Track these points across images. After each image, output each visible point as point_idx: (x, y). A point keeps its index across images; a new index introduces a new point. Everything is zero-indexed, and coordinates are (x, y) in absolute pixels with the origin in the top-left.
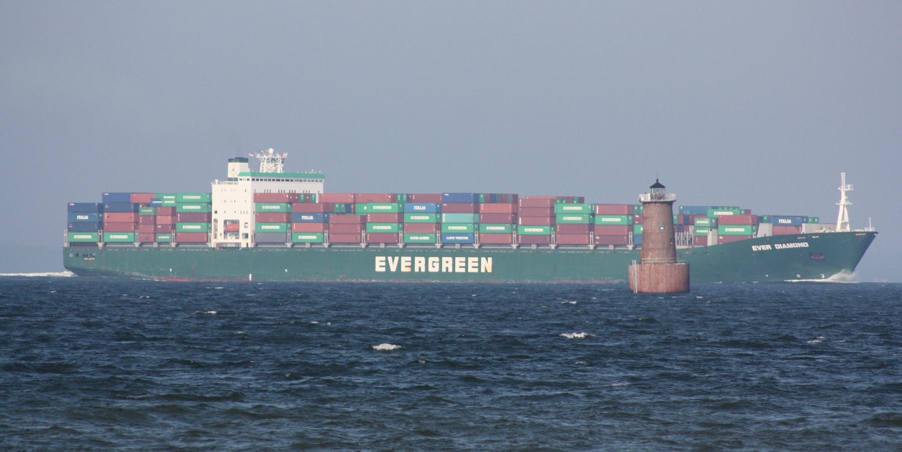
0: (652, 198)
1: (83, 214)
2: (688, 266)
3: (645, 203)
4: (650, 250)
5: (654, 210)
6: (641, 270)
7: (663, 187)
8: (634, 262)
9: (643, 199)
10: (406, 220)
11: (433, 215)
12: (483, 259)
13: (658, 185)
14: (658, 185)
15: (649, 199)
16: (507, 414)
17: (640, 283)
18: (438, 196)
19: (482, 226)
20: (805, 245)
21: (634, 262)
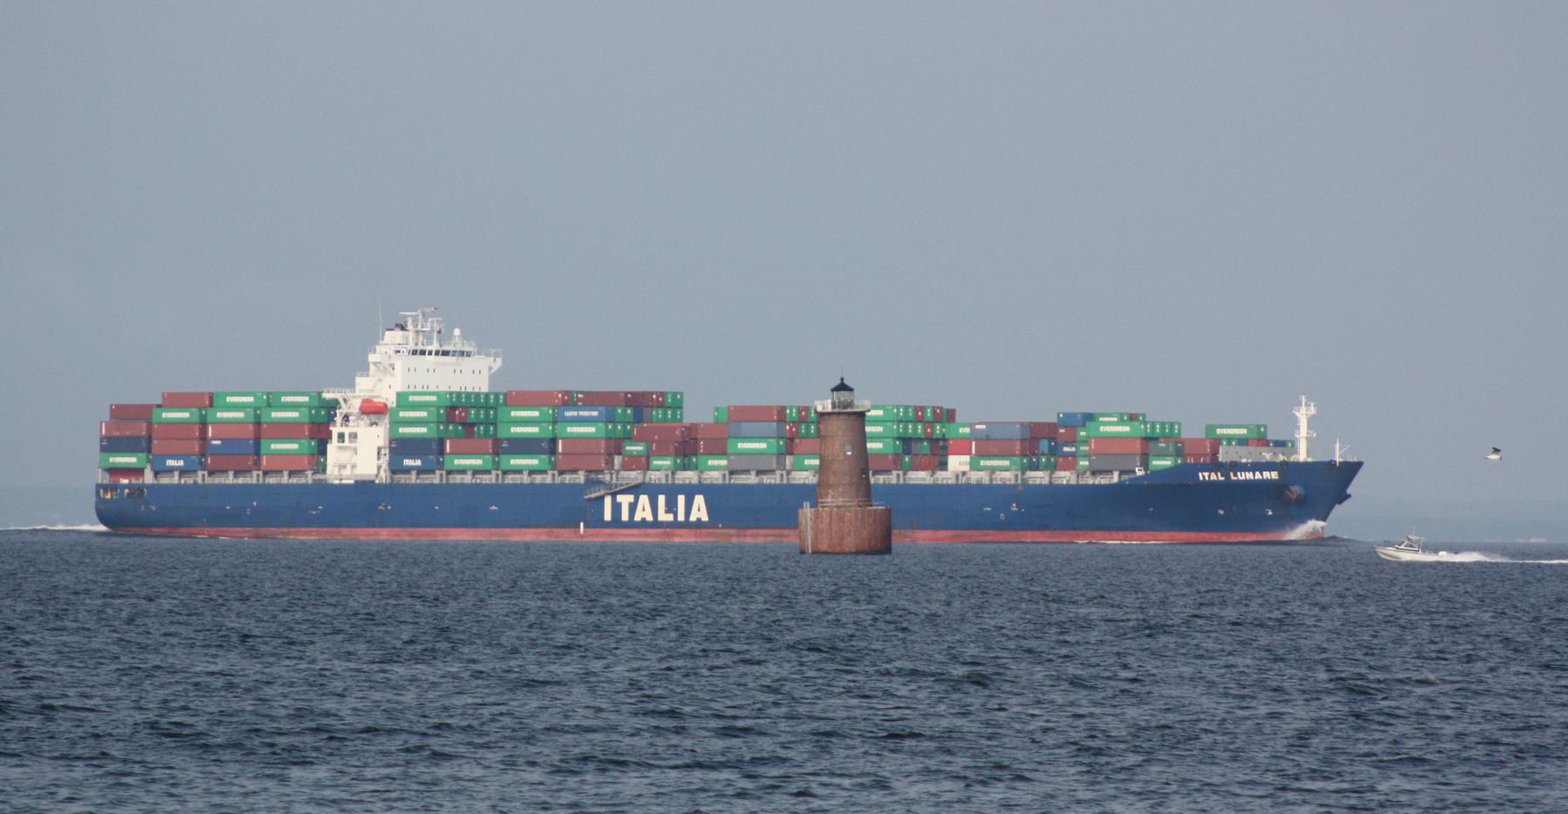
0: (834, 406)
1: (412, 456)
2: (888, 512)
3: (822, 415)
4: (830, 486)
5: (837, 427)
6: (817, 516)
7: (851, 390)
8: (807, 505)
9: (820, 409)
10: (263, 450)
11: (773, 441)
12: (650, 518)
13: (842, 387)
14: (842, 387)
15: (829, 409)
16: (1462, 674)
17: (815, 539)
18: (201, 395)
19: (504, 458)
20: (1274, 475)
21: (807, 505)
